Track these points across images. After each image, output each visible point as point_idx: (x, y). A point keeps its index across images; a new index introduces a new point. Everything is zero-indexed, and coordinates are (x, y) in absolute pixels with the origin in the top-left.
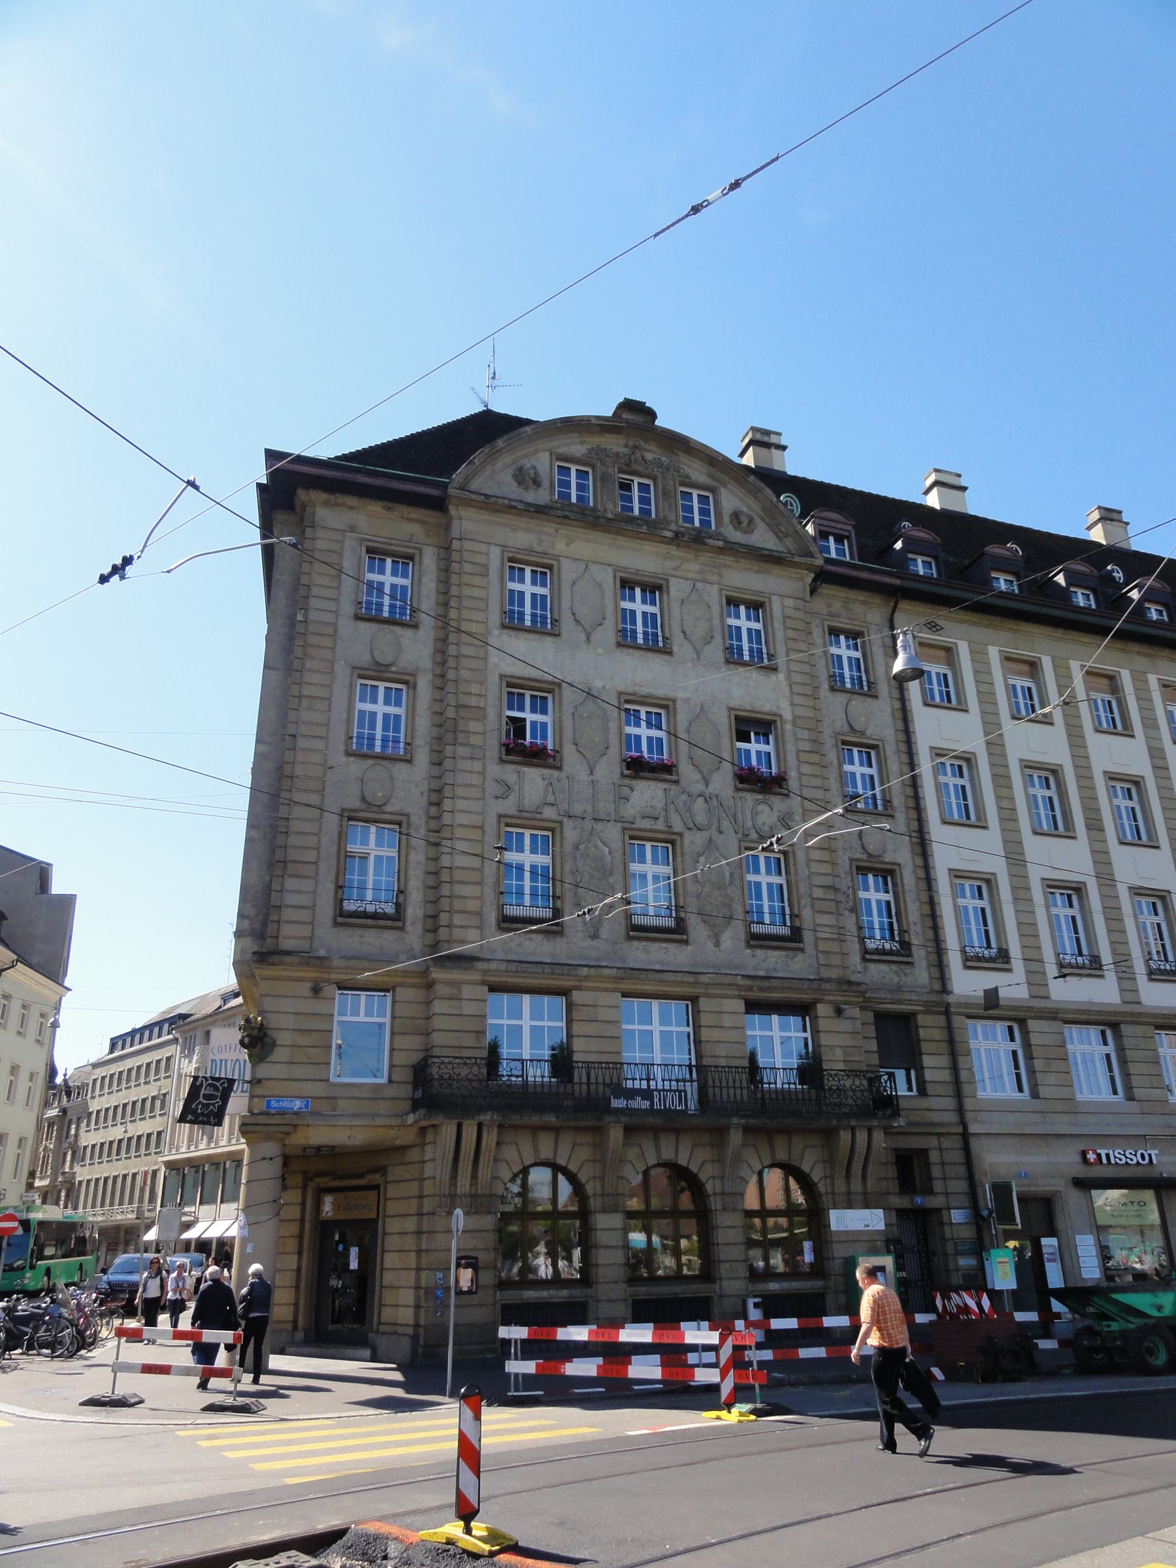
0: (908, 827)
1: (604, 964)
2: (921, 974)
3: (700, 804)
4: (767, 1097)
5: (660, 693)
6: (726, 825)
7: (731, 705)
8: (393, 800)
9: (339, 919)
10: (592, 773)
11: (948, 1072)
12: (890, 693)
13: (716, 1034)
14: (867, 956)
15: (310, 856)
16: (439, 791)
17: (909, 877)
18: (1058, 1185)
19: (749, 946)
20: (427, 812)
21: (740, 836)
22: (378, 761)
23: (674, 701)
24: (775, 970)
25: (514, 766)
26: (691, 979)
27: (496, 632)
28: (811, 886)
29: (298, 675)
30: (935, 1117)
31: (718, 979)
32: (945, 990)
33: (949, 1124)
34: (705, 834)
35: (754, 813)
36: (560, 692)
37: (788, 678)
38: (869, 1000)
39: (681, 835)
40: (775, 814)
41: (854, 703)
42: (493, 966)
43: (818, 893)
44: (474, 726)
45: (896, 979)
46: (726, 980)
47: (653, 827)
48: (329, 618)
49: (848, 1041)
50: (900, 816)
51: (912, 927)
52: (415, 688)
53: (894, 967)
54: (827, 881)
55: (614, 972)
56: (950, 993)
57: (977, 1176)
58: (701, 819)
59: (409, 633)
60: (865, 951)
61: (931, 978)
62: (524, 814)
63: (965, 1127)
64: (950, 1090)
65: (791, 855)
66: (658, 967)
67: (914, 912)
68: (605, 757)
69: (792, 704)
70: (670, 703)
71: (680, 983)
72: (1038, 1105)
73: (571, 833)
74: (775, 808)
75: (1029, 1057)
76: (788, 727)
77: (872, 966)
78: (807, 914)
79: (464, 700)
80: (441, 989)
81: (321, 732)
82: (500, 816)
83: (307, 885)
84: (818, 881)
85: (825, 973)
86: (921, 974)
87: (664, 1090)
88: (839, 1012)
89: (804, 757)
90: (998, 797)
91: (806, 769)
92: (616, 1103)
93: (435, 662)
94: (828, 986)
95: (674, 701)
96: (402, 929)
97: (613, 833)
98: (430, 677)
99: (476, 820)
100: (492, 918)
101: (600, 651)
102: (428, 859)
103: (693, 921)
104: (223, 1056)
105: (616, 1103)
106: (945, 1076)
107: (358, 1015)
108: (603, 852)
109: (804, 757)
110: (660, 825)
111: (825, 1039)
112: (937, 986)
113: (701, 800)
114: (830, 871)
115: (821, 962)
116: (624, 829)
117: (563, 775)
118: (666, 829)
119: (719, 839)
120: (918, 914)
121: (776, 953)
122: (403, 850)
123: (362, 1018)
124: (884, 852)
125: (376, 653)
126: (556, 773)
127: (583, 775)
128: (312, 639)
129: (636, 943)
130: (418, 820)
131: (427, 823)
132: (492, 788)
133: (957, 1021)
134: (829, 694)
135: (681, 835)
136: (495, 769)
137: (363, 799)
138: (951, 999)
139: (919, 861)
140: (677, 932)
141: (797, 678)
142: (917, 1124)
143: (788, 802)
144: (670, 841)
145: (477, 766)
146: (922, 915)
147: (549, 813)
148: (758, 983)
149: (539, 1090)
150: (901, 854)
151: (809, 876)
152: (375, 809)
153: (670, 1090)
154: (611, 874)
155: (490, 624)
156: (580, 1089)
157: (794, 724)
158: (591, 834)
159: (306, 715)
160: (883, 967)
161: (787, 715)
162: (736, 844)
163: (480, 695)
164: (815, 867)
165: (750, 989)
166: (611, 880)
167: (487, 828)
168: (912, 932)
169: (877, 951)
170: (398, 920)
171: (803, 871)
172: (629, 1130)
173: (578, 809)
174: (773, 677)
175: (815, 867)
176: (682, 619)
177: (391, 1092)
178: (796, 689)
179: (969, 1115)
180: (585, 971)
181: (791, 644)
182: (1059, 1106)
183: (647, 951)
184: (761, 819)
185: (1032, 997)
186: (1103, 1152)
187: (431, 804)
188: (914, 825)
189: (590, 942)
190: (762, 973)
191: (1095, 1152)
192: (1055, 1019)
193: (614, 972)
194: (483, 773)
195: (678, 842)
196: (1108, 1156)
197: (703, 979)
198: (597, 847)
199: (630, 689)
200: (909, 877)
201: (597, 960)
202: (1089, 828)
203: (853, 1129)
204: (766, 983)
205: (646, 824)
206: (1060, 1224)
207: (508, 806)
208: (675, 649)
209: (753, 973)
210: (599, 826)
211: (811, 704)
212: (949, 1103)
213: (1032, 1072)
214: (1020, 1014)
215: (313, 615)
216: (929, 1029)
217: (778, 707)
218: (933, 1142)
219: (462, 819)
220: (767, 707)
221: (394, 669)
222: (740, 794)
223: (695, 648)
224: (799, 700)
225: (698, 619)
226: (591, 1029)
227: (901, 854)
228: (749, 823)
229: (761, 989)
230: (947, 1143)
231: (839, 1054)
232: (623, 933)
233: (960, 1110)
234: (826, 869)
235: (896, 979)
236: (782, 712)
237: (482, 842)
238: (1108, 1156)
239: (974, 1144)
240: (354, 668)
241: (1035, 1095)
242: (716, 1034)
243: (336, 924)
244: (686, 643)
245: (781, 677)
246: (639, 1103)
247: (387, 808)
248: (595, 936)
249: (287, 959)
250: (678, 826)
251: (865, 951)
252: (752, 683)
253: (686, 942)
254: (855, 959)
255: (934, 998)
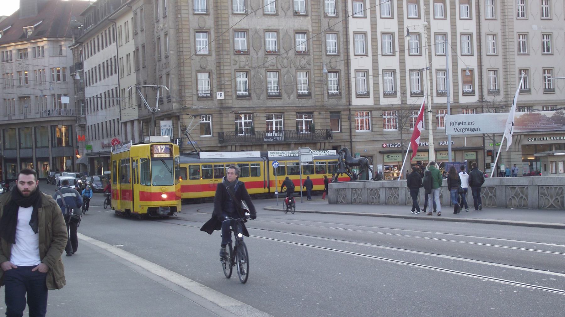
0: (344, 58)
1: (261, 106)
2: (344, 101)
3: (285, 60)
4: (300, 135)
5: (275, 28)
6: (292, 65)
7: (295, 29)
8: (208, 66)
9: (199, 99)
10: (257, 55)
11: (348, 126)
12: (342, 15)
13: (289, 121)
14: (329, 97)
15: (190, 83)
16: (219, 63)
17: (343, 74)
18: (376, 153)
19: (297, 98)
20: (216, 69)
21: (296, 68)
22: (203, 56)
23: (279, 30)
24: (304, 104)
25: (237, 55)
26: (282, 108)
27: (231, 16)
28: (315, 80)
29: (181, 34)
30: (344, 138)
31: (289, 108)
32: (350, 105)
33: (347, 139)
34: (287, 69)
35: (300, 61)
36: (249, 32)
37: (311, 18)
38: (327, 109)
39: (280, 70)
40: (306, 61)
41: (331, 21)
42: (236, 109)
43: (316, 82)
44: (227, 45)
45: (336, 102)
46: (291, 108)
47: (274, 68)
48: (186, 15)
49: (321, 121)
50: (342, 55)
51: (342, 87)
52: (210, 33)
53: (336, 99)
54: (319, 78)
55: (264, 108)
56: (351, 105)
57: (353, 152)
58: (286, 65)
59: (207, 17)
60: (329, 95)
61: (346, 101)
62: (241, 69)
63: (351, 140)
64: (349, 130)
65: (310, 72)
66: (274, 106)
67: (343, 83)
68: (260, 50)
69: (312, 26)
70: (278, 31)
71: (280, 110)
72: (373, 133)
73: (252, 73)
74: (306, 59)
75: (372, 121)
76: (311, 34)
77: (330, 99)
78: (313, 88)
79: (224, 38)
80: (224, 115)
81: (189, 50)
82: (235, 70)
83: (190, 91)
84: (316, 79)
85: (317, 104)
86: (344, 101)
87: (276, 136)
88: (320, 113)
89: (315, 43)
90: (372, 45)
91: (315, 46)
92: (265, 140)
93: (214, 25)
94: (317, 108)
95: (279, 30)
96: (213, 100)
97: (263, 71)
98: (214, 29)
99: (229, 71)
100: (234, 96)
101: (259, 17)
102: (217, 81)
103: (283, 92)
104: (164, 128)
105: (265, 140)
106: (348, 127)
107: (204, 121)
108: (261, 77)
109: (315, 43)
110: (275, 68)
111: (316, 121)
112: (348, 104)
113: (286, 59)
114: (320, 76)
115: (316, 101)
116: (266, 70)
117: (250, 56)
118: (276, 68)
119: (290, 70)
120: (344, 84)
121: (304, 99)
122: (211, 80)
123: (205, 122)
124: (336, 66)
125: (200, 25)
126: (248, 56)
127: (255, 56)
128: (184, 23)
129: (269, 100)
130: (214, 71)
131: (216, 71)
132: (232, 62)
133: (352, 113)
134: (323, 18)
135: (280, 70)
136: (233, 57)
137: (201, 67)
138: (351, 107)
139: (346, 68)
140: (279, 96)
141: (314, 17)
142: (338, 140)
143: (310, 57)
144: (278, 71)
145: (228, 57)
146: (346, 84)
147: (247, 67)
148: (299, 108)
149: (248, 137)
150: (341, 67)
151: (314, 78)
152: (204, 69)
153: (278, 136)
154: (263, 82)
155: (229, 14)
156: (257, 137)
157: (312, 33)
158: (258, 72)
159: (185, 45)
160: (333, 100)
161: (311, 30)
162: (295, 70)
163: (228, 36)
164: (316, 75)
165: (297, 110)
166: (263, 84)
167: (232, 73)
168: (342, 89)
169: (333, 95)
170: (212, 98)
171: (313, 76)
172: (268, 145)
173: (254, 65)
174: (307, 18)
175: (316, 75)
176: (281, 3)
177: (213, 138)
178: (314, 21)
179: (353, 137)
180: (257, 109)
181: (313, 7)
182: (378, 133)
183: (272, 102)
184: (302, 62)
185: (375, 104)
186: (388, 144)
187: (217, 66)
188: (346, 57)
189: (258, 101)
190: (300, 105)
191: (386, 144)
192: (380, 110)
193: (264, 108)
194: (230, 58)
195: (280, 72)
196: (389, 145)
197: (286, 108)
198: (259, 76)
199: (267, 28)
200: (343, 74)
201: (260, 105)
202: (400, 51)
203: (321, 143)
204: (301, 108)
205: (271, 68)
206: (374, 162)
207: (237, 67)
208: (279, 13)
209: (298, 105)
210: (259, 70)
211: (317, 25)
212: (348, 134)
213: (372, 125)
214: (370, 110)
215: (183, 15)
216: (344, 115)
217: (308, 28)
218: (343, 144)
219: (226, 72)
220: (305, 28)
221: (204, 29)
222: (296, 56)
223: (285, 12)
224: (314, 25)
225: (286, 2)
226: (259, 122)
227: (341, 67)
228: (298, 64)
229: (300, 110)
230: (346, 144)
231: (319, 124)
232: (266, 97)
233: (351, 136)
234: (319, 75)
235: (336, 102)
236: (309, 29)
237: (231, 77)
238: (389, 145)
239: (353, 144)
240: (195, 30)
241: (372, 131)
242: (289, 121)
243: (198, 100)
244: (282, 11)
245: (309, 17)
246: (271, 140)
247: (207, 69)
248: (259, 99)
249: (189, 110)
250: (280, 67)
251: (329, 95)
252: (301, 21)
253: (281, 99)
254: (326, 98)
255: (346, 107)
